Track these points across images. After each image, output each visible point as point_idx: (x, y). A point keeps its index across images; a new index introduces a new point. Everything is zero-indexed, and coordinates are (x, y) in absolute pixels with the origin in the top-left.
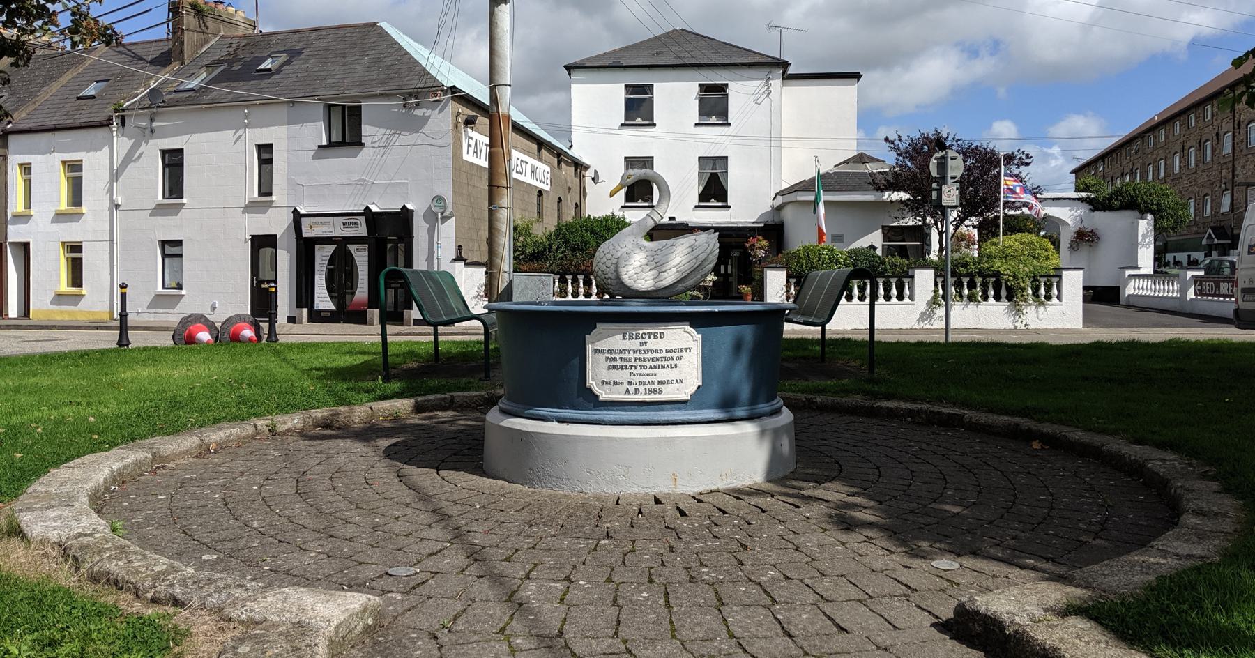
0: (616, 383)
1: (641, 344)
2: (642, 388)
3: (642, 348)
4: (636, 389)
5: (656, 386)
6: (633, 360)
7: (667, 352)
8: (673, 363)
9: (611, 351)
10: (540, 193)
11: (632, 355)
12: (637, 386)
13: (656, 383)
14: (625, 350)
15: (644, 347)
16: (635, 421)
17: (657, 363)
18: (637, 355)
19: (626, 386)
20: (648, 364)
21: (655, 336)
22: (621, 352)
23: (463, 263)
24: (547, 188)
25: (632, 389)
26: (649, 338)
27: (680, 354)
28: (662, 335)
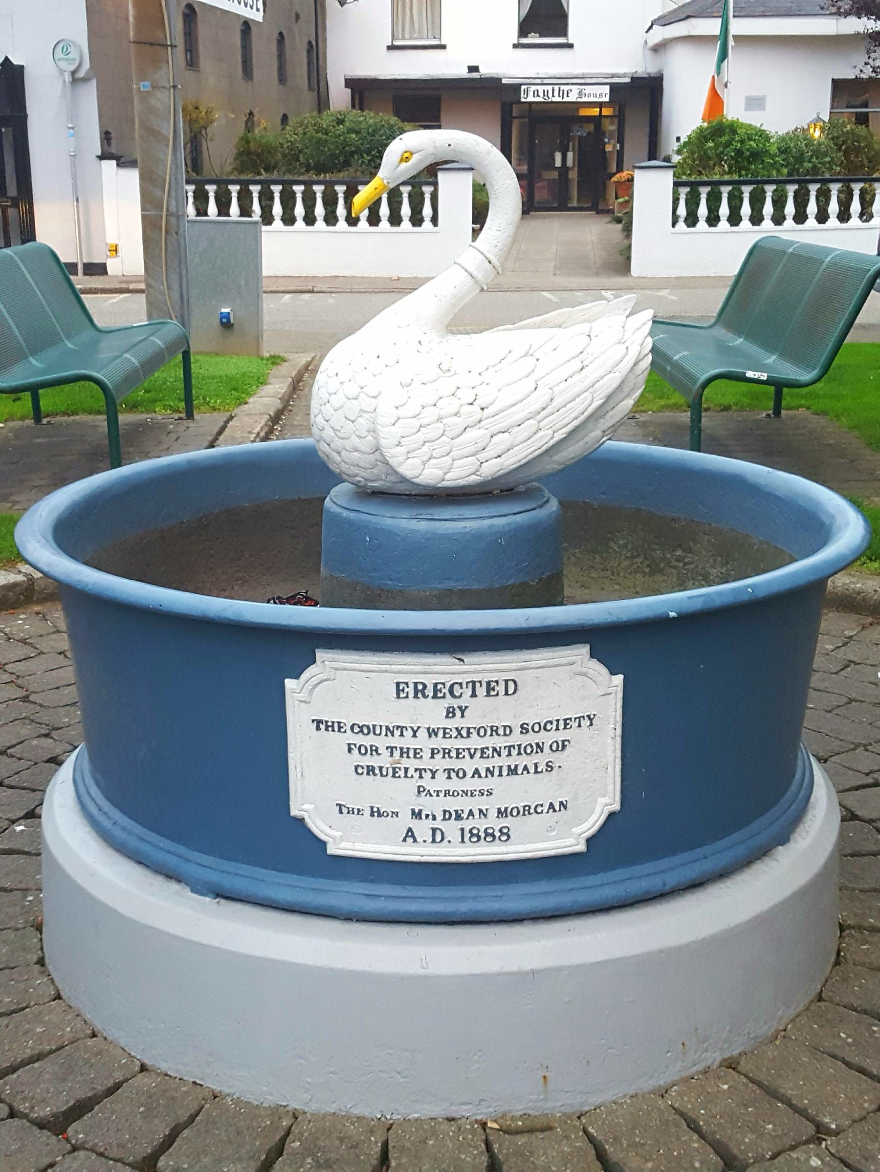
0: (376, 813)
1: (450, 713)
2: (452, 828)
3: (452, 724)
4: (434, 830)
5: (494, 823)
6: (427, 754)
7: (524, 729)
8: (541, 759)
9: (363, 730)
10: (247, 26)
11: (423, 742)
12: (438, 824)
13: (493, 813)
14: (402, 728)
15: (457, 722)
16: (430, 914)
17: (495, 762)
18: (439, 742)
19: (406, 821)
20: (468, 765)
21: (489, 688)
22: (390, 731)
23: (114, 162)
24: (258, 17)
25: (422, 829)
26: (474, 695)
27: (561, 736)
28: (512, 687)
